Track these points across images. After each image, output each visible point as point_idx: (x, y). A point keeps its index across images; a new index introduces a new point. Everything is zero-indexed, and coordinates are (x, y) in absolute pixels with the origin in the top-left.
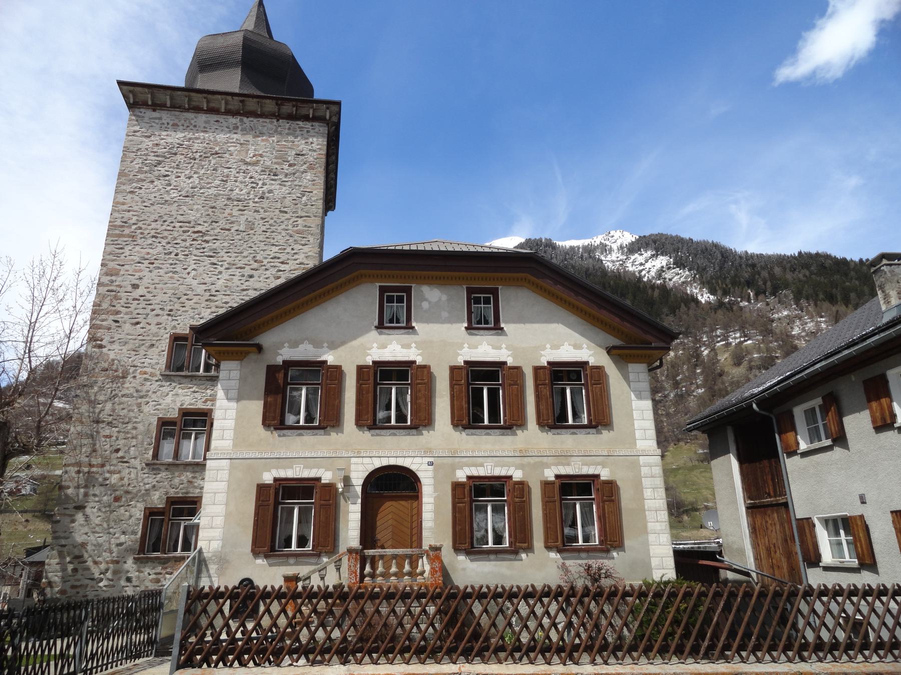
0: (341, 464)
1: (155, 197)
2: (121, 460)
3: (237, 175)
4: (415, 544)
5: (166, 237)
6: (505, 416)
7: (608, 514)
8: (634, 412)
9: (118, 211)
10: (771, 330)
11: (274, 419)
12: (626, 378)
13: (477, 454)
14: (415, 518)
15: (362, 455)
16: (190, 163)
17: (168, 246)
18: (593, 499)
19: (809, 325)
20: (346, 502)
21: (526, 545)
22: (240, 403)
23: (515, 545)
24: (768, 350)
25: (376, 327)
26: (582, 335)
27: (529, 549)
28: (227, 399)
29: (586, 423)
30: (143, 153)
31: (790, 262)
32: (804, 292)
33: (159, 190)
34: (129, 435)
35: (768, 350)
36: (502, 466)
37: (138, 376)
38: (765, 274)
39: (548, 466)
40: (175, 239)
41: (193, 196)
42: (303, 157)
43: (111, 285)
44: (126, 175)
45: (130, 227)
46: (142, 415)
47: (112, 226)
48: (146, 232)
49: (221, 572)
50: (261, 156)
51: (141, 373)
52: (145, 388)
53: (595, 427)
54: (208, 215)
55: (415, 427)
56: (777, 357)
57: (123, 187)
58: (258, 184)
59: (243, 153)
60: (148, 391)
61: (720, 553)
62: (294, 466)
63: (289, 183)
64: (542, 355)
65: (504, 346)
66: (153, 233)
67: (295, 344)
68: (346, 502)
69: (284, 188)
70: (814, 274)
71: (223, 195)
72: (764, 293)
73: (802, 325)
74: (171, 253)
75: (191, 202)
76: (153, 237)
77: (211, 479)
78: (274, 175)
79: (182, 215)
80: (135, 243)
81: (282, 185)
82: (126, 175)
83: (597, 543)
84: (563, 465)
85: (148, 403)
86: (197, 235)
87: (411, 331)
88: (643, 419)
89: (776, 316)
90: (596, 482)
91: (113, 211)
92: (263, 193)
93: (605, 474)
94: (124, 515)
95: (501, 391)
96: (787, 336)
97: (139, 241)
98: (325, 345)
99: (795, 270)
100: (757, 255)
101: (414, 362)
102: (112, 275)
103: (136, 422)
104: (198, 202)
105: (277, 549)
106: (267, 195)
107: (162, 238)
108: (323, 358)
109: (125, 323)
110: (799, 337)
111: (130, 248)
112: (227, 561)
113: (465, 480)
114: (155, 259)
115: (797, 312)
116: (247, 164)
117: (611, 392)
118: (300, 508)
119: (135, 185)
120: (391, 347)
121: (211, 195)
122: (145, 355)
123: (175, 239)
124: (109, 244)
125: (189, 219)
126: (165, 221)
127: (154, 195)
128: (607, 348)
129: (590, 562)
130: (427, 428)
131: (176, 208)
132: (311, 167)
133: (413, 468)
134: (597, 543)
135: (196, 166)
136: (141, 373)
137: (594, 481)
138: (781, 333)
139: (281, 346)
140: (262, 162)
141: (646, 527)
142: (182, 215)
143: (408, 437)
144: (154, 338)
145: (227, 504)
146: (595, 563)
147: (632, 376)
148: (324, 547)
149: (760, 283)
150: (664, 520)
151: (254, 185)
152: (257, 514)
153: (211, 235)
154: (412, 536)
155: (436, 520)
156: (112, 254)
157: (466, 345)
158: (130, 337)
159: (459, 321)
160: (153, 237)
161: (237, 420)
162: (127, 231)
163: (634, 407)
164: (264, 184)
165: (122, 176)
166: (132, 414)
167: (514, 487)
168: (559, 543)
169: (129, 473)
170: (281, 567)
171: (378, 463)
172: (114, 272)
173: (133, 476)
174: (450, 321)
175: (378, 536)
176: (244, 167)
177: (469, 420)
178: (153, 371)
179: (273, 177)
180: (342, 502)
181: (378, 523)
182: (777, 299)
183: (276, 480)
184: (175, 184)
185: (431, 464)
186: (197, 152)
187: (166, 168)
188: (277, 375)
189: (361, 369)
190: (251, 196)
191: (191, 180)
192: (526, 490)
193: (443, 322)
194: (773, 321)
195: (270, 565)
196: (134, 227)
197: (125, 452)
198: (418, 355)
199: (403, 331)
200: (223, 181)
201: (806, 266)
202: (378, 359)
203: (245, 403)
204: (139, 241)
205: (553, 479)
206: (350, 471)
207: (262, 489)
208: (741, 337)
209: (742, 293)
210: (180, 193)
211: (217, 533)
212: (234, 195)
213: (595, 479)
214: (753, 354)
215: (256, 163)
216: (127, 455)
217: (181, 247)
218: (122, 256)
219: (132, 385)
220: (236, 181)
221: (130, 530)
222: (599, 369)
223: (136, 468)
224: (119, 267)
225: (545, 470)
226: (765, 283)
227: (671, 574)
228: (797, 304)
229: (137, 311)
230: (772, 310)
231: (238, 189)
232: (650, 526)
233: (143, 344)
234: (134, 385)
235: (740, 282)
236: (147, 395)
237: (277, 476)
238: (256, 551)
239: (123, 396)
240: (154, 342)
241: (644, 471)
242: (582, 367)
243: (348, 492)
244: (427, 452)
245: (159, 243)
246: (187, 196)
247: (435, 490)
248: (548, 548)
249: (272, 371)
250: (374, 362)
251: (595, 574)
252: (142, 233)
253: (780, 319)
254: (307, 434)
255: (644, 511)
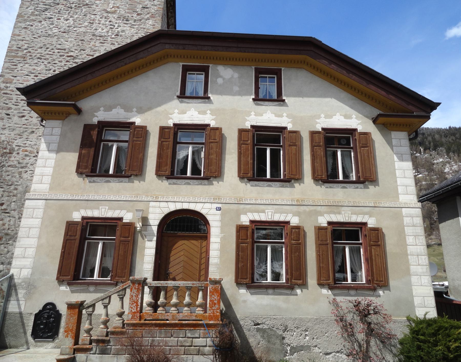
0: (141, 206)
1: (42, 32)
2: (4, 211)
3: (101, 19)
4: (202, 278)
5: (48, 59)
6: (284, 171)
7: (375, 257)
8: (397, 171)
9: (15, 40)
10: (433, 169)
11: (86, 167)
12: (389, 143)
13: (259, 202)
14: (204, 255)
15: (159, 200)
16: (68, 10)
17: (48, 65)
18: (361, 244)
19: (454, 167)
20: (143, 239)
21: (301, 281)
22: (58, 154)
23: (291, 281)
24: (431, 180)
25: (178, 97)
26: (352, 107)
27: (304, 285)
28: (48, 151)
29: (354, 179)
30: (35, 3)
31: (444, 132)
32: (452, 149)
33: (45, 27)
34: (11, 194)
35: (431, 180)
36: (281, 213)
37: (21, 153)
38: (430, 138)
39: (322, 214)
40: (54, 60)
41: (69, 32)
42: (147, 10)
43: (6, 90)
44: (22, 16)
45: (23, 51)
46: (22, 180)
47: (10, 50)
48: (34, 55)
49: (28, 296)
50: (118, 7)
51: (23, 151)
52: (25, 161)
53: (363, 182)
54: (79, 45)
55: (206, 178)
56: (436, 184)
57: (19, 24)
58: (114, 26)
59: (106, 5)
60: (28, 164)
61: (447, 293)
62: (100, 207)
63: (137, 26)
64: (317, 123)
65: (285, 114)
66: (38, 55)
67: (109, 108)
68: (143, 239)
69: (133, 29)
70: (458, 139)
71: (90, 32)
72: (429, 149)
73: (450, 167)
74: (50, 69)
75: (67, 36)
76: (38, 58)
77: (27, 216)
78: (126, 21)
79: (60, 44)
80: (25, 62)
81: (132, 26)
82: (22, 16)
83: (364, 282)
84: (335, 213)
85: (27, 172)
86: (69, 58)
87: (207, 100)
88: (405, 177)
89: (435, 161)
90: (363, 229)
91: (12, 40)
92: (118, 32)
93: (372, 223)
94: (3, 250)
95: (281, 152)
96: (442, 172)
97: (28, 61)
98: (135, 110)
99: (447, 136)
100: (425, 128)
101: (208, 125)
102: (7, 83)
103: (17, 185)
104: (72, 36)
105: (81, 278)
106: (121, 33)
107: (45, 59)
108: (132, 120)
109: (14, 116)
110: (448, 173)
111: (22, 65)
112: (35, 287)
113: (248, 223)
114: (39, 73)
115: (447, 160)
116: (108, 12)
117: (377, 154)
118: (104, 244)
119: (28, 23)
120: (189, 113)
121: (81, 32)
122: (27, 138)
123: (54, 60)
124: (6, 62)
125: (65, 48)
126: (47, 48)
127: (41, 30)
128: (373, 118)
129: (360, 299)
130: (217, 179)
131: (56, 40)
132: (153, 16)
133: (203, 212)
134: (364, 282)
135: (72, 12)
136: (23, 151)
137: (361, 228)
138: (439, 171)
139: (98, 110)
140: (118, 12)
141: (408, 270)
142: (60, 44)
143: (200, 186)
144: (34, 127)
145: (39, 238)
146: (364, 300)
147: (394, 142)
148: (121, 277)
149: (427, 143)
150: (425, 264)
151: (112, 27)
152: (64, 247)
153: (79, 59)
154: (200, 271)
155: (221, 257)
156: (8, 69)
157: (253, 113)
158: (17, 126)
159: (248, 93)
160: (38, 58)
161: (54, 168)
162: (20, 54)
163: (396, 167)
164: (119, 26)
165: (20, 17)
166: (14, 179)
167: (291, 231)
168: (331, 281)
169: (10, 221)
170: (82, 294)
171: (173, 207)
172: (9, 81)
173: (12, 223)
174: (240, 93)
175: (171, 270)
176: (105, 15)
177: (254, 174)
178: (32, 149)
179: (126, 22)
180: (140, 238)
181: (171, 259)
182: (436, 152)
183: (83, 218)
184: (56, 24)
185: (219, 209)
186: (73, 3)
187: (51, 13)
188: (92, 132)
189: (163, 129)
190: (110, 34)
191: (68, 21)
192: (302, 233)
193: (234, 95)
194: (434, 164)
195: (72, 292)
196: (25, 51)
197: (8, 206)
198: (212, 120)
199: (200, 100)
200: (90, 23)
201: (454, 134)
202: (178, 122)
203: (62, 154)
204: (28, 61)
205: (326, 225)
206: (148, 213)
207: (70, 225)
208: (415, 173)
209: (416, 148)
210: (60, 30)
211: (28, 262)
212: (97, 33)
213: (363, 226)
214: (422, 182)
215: (114, 12)
216: (9, 208)
217: (58, 66)
218: (16, 70)
219: (16, 159)
220: (99, 24)
221: (7, 262)
222: (367, 135)
223: (15, 217)
224: (12, 78)
225: (319, 217)
226: (430, 143)
227: (433, 314)
228: (448, 155)
229: (24, 108)
230: (433, 158)
231: (100, 29)
232: (413, 269)
233: (26, 131)
234: (18, 159)
235: (416, 143)
236: (26, 167)
237: (85, 215)
238: (61, 279)
239: (9, 166)
240: (34, 130)
241: (407, 220)
242: (352, 134)
243: (146, 230)
244: (215, 199)
245: (43, 62)
246: (65, 32)
247: (222, 232)
248: (321, 285)
249: (88, 128)
250: (174, 125)
251: (364, 310)
252: (30, 56)
253: (438, 163)
254: (114, 181)
255: (407, 255)
